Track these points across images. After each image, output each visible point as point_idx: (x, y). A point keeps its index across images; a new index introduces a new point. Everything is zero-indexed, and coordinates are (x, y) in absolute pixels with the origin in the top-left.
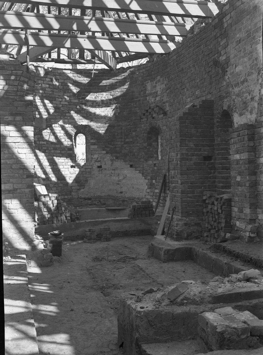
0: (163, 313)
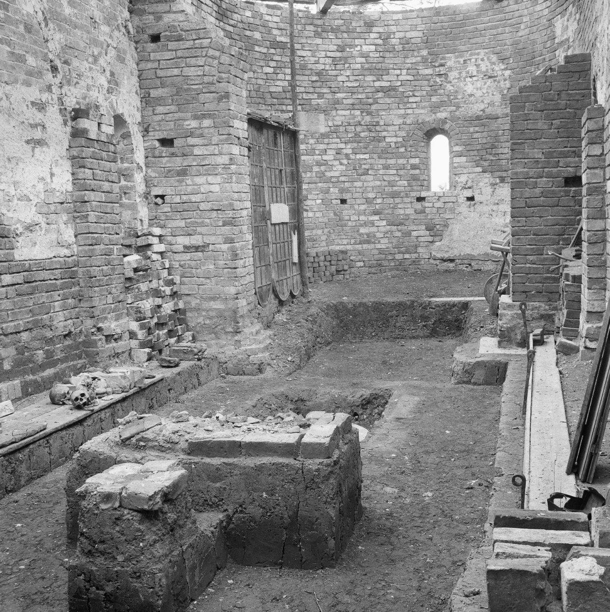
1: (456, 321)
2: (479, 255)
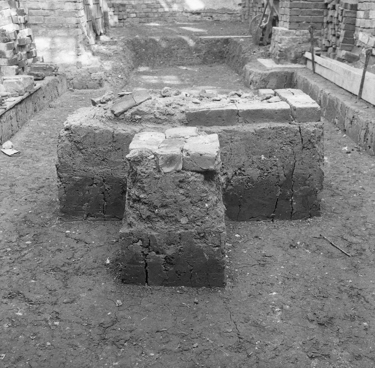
0: (97, 132)
1: (220, 52)
2: (218, 9)
